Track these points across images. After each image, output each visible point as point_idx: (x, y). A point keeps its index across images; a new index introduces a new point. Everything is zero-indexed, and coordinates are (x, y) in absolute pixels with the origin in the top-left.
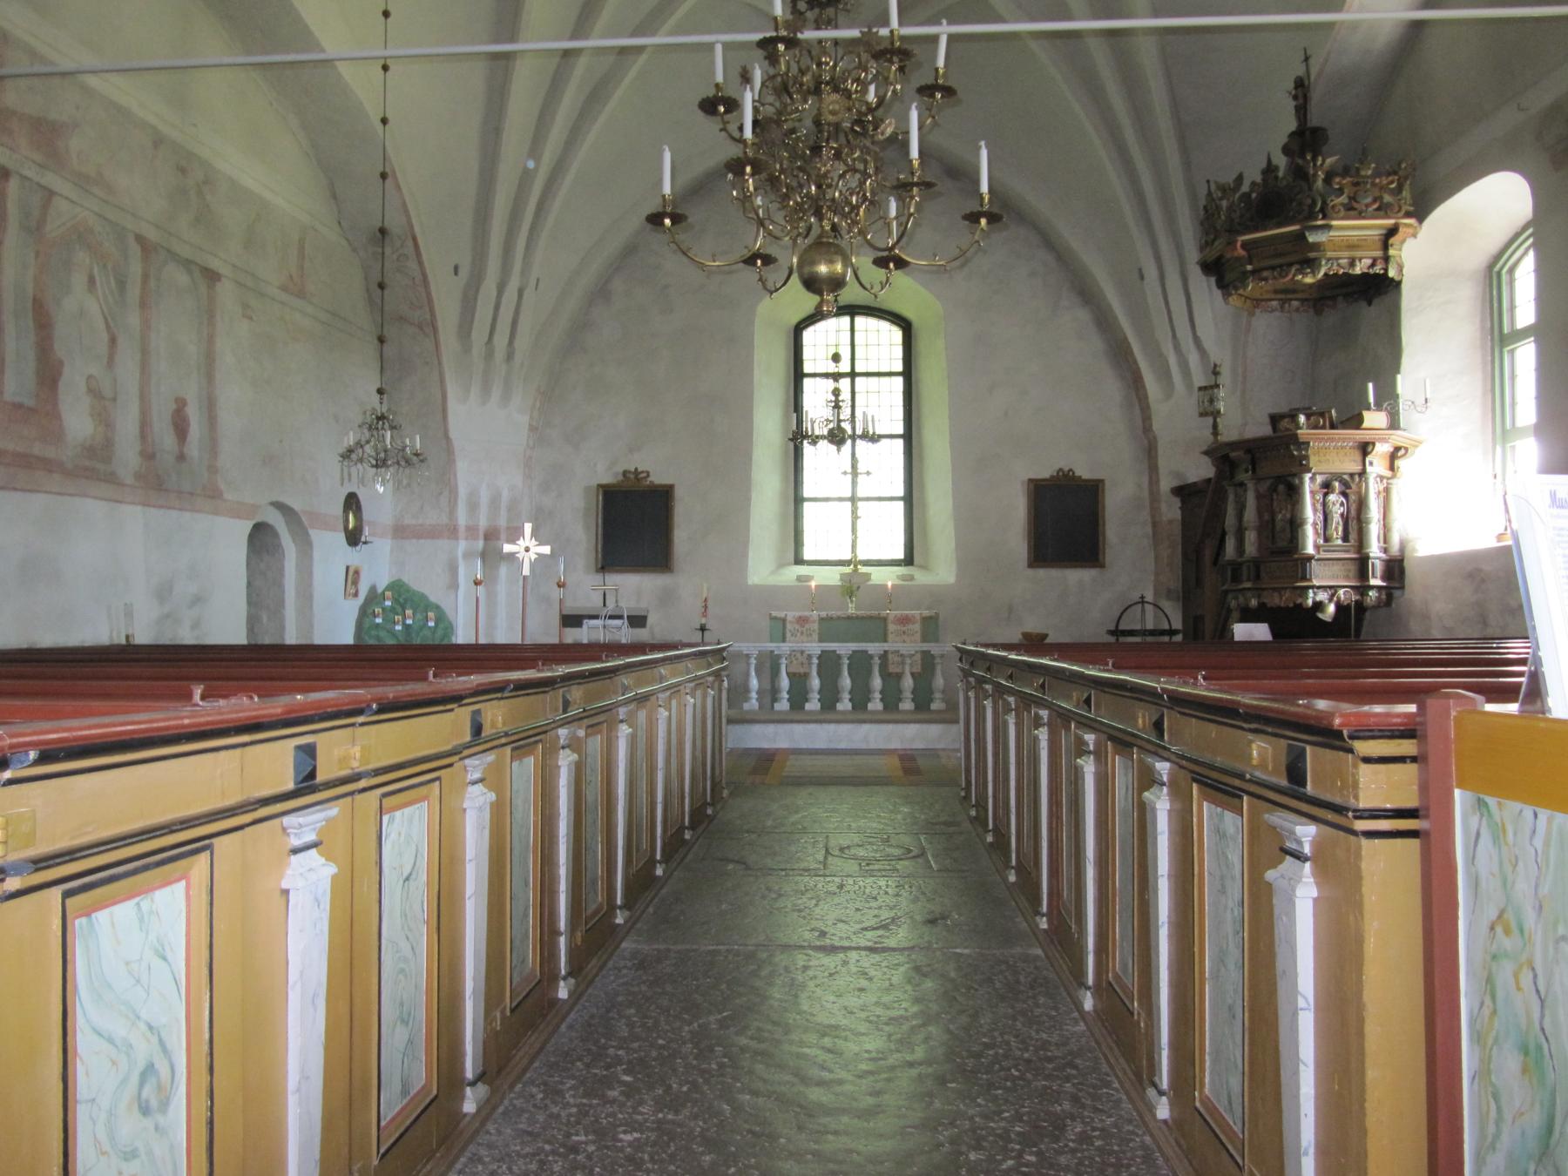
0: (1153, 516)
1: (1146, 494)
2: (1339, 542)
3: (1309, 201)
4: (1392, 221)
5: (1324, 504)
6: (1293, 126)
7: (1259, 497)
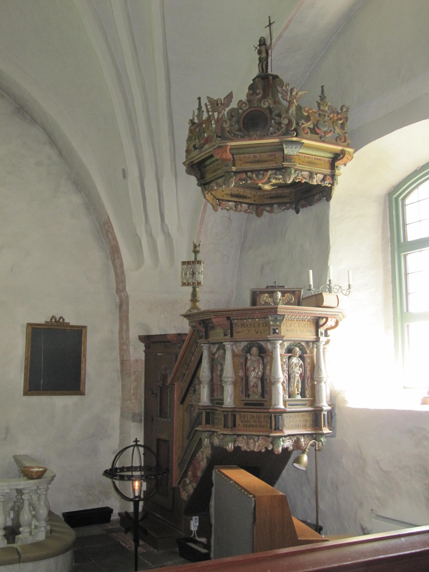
0: (122, 356)
1: (117, 337)
2: (299, 397)
3: (286, 121)
4: (340, 148)
5: (289, 366)
6: (256, 72)
7: (234, 355)
